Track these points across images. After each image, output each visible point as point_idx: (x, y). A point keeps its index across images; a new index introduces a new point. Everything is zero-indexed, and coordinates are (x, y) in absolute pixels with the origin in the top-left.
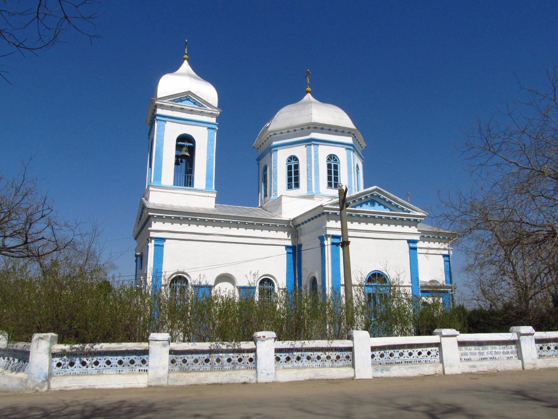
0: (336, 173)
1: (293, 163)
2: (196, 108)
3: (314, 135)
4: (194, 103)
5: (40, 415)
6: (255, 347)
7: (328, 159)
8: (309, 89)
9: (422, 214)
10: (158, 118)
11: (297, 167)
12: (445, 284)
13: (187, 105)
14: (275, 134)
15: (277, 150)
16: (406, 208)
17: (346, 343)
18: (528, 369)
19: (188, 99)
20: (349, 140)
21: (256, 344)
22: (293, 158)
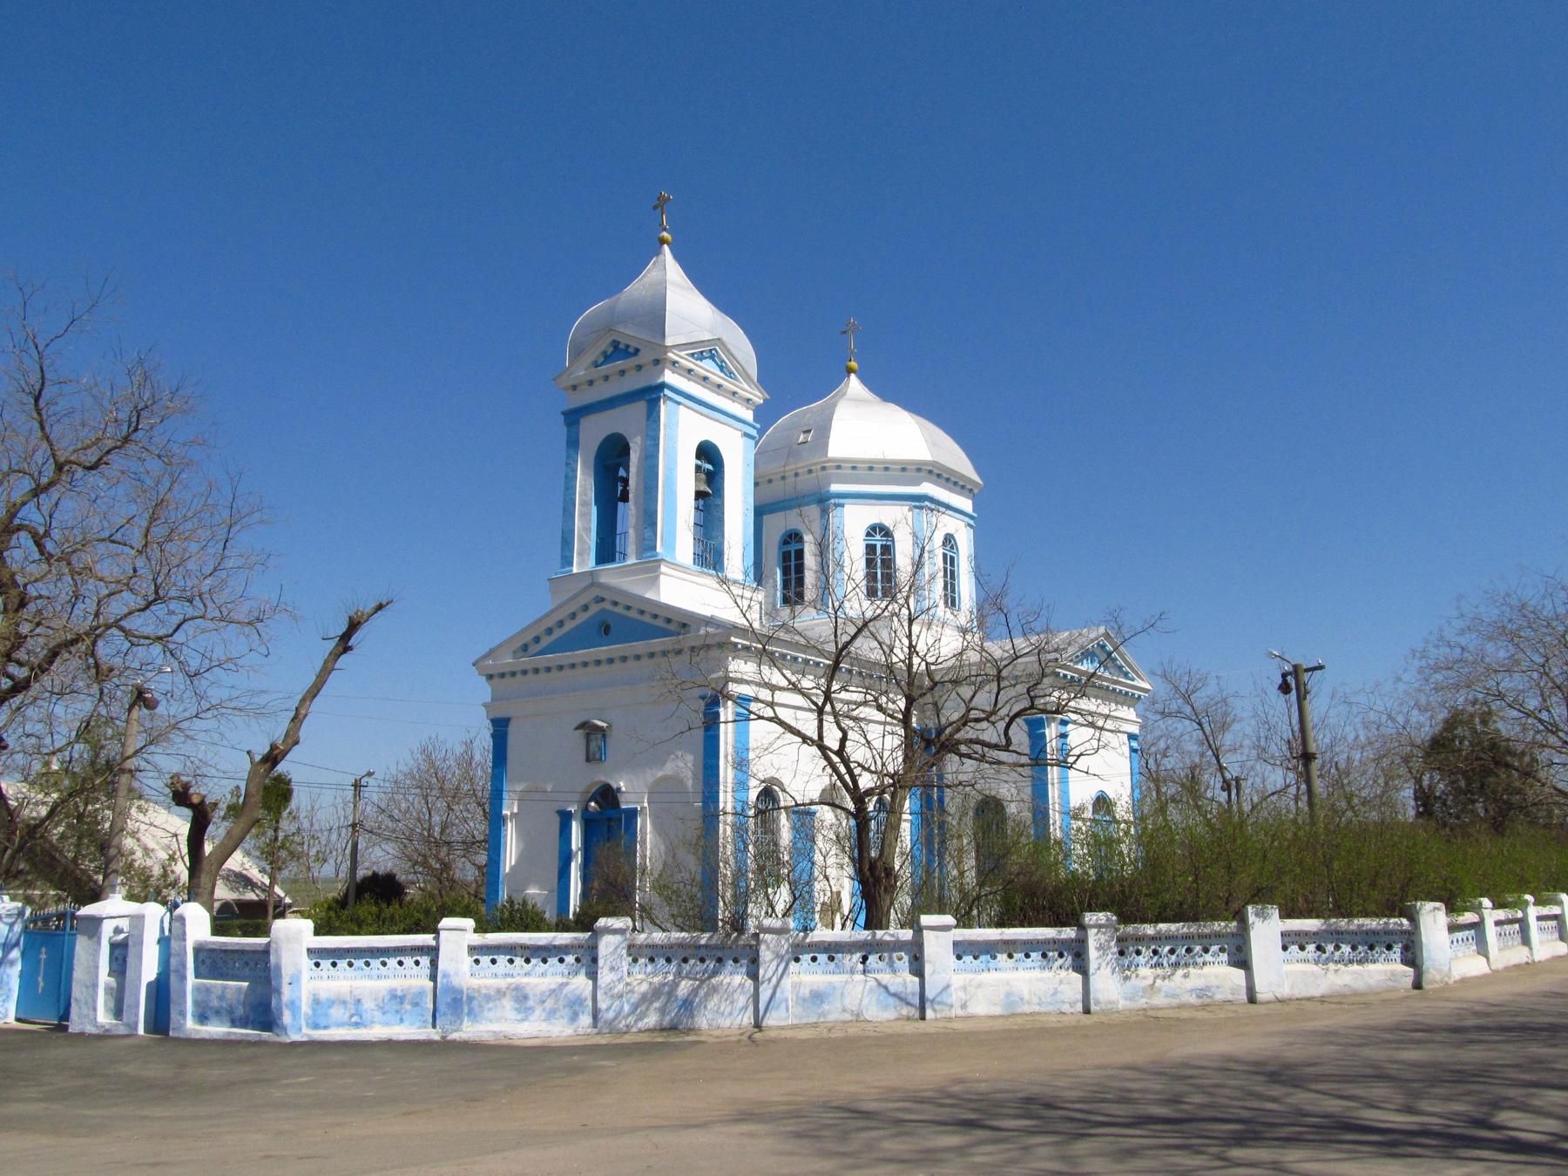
0: (953, 577)
1: (878, 541)
2: (716, 376)
3: (928, 488)
4: (721, 368)
5: (1157, 1093)
6: (434, 943)
7: (868, 534)
8: (854, 364)
9: (1147, 686)
10: (667, 392)
11: (887, 549)
12: (1010, 823)
13: (708, 367)
14: (839, 467)
15: (842, 506)
16: (1132, 674)
17: (426, 939)
18: (1285, 991)
19: (712, 357)
20: (966, 504)
21: (437, 939)
22: (885, 532)
